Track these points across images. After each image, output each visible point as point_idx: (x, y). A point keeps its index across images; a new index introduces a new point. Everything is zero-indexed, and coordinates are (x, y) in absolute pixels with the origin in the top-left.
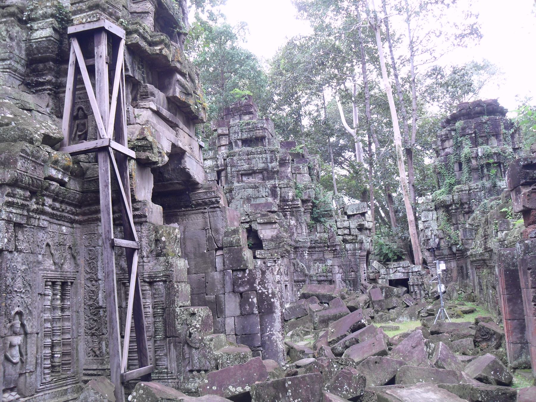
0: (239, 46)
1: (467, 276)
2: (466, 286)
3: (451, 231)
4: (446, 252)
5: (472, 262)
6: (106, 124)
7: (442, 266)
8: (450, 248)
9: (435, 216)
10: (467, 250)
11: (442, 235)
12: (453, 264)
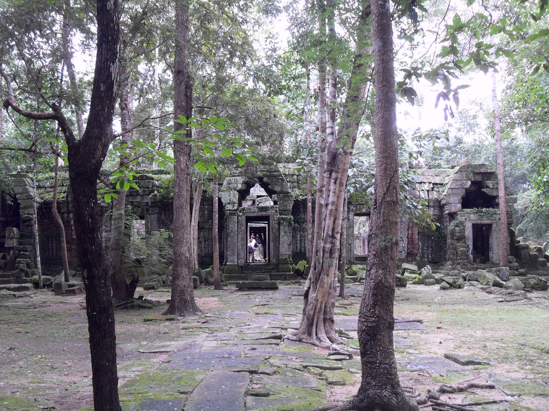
6: (255, 286)
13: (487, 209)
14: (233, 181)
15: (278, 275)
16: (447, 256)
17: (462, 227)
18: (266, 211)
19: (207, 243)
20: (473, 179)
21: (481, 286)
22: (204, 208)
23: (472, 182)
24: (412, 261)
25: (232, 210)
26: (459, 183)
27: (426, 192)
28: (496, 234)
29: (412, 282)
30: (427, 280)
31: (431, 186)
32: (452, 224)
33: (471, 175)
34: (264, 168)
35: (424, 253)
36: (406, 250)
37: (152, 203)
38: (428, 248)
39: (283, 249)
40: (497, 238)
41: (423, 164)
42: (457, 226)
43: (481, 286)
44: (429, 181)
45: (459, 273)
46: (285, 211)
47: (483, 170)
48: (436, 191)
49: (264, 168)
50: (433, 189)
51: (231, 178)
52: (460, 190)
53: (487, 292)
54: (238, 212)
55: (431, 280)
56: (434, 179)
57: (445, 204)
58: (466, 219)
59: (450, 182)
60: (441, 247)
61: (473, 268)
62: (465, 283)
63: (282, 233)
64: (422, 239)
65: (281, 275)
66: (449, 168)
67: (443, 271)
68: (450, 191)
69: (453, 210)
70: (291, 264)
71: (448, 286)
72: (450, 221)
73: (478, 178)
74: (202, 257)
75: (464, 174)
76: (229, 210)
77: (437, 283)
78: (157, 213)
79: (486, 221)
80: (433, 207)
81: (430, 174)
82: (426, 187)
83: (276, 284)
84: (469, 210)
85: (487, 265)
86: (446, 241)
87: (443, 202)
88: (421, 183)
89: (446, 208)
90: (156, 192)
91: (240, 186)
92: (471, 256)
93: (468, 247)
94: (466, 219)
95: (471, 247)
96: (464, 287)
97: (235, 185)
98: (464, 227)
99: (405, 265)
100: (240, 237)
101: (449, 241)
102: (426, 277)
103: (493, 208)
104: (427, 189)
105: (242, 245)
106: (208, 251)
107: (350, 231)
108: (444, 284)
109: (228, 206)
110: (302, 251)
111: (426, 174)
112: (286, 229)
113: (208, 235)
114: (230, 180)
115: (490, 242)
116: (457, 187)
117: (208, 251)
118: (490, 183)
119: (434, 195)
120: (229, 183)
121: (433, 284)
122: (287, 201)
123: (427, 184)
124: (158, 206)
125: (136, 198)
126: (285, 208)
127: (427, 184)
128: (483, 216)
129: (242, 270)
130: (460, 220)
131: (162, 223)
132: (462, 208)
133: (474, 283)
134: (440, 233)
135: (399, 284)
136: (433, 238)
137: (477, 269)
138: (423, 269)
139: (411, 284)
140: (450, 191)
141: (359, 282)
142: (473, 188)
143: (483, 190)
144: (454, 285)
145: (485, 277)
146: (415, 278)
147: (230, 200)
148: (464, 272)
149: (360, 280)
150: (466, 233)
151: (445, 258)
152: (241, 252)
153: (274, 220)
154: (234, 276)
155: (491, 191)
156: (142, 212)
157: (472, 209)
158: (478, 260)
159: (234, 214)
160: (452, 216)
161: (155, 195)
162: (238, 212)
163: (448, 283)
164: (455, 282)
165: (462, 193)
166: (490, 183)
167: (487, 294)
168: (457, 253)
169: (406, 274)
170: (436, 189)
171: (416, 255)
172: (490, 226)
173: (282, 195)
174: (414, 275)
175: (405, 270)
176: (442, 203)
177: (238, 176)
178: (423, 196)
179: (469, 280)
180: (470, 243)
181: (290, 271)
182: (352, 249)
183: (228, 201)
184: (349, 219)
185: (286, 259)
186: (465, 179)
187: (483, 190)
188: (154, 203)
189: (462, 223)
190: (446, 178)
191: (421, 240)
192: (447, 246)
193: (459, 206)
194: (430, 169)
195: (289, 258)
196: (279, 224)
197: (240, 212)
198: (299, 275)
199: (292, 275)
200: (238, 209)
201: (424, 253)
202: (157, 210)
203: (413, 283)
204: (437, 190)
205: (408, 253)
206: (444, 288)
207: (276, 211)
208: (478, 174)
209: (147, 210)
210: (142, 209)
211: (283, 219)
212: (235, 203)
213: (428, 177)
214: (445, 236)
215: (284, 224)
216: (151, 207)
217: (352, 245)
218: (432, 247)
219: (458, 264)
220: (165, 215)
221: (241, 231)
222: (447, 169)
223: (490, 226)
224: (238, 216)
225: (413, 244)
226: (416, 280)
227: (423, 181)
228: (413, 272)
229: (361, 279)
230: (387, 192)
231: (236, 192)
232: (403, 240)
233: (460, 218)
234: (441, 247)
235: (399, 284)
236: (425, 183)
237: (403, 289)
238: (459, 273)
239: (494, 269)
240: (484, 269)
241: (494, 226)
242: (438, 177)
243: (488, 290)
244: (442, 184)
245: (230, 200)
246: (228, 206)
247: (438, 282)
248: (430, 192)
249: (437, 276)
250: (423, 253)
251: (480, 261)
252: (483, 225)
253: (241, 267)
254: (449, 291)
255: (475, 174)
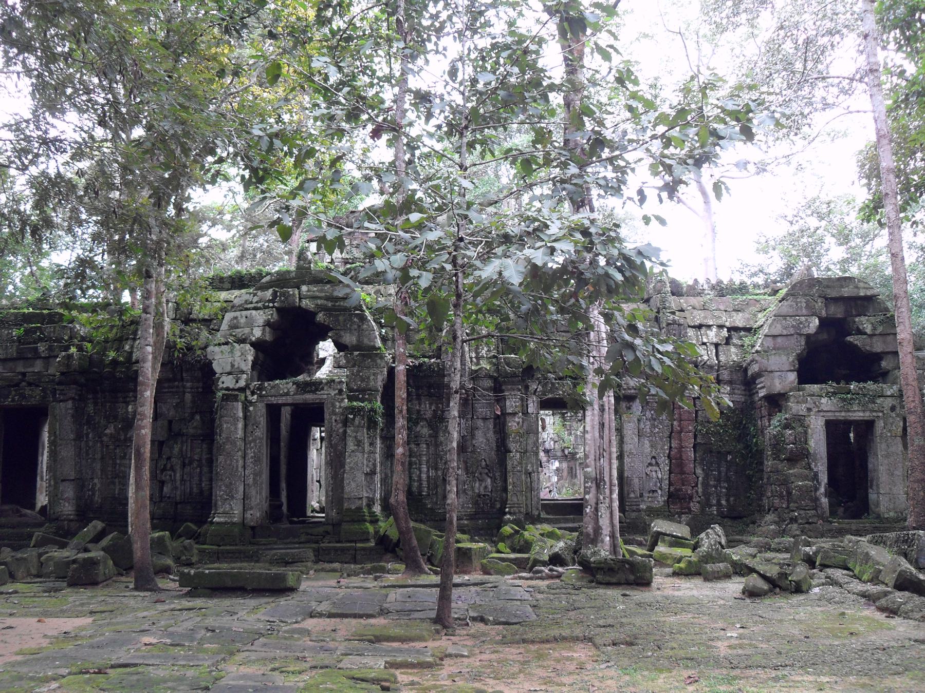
0: (731, 149)
1: (576, 476)
2: (574, 484)
3: (565, 435)
4: (559, 454)
5: (580, 464)
6: (229, 583)
7: (557, 464)
8: (563, 451)
9: (552, 421)
10: (576, 453)
11: (557, 439)
12: (565, 465)
13: (862, 385)
14: (243, 321)
15: (336, 550)
16: (765, 501)
17: (800, 429)
18: (314, 392)
19: (187, 469)
20: (824, 313)
21: (861, 587)
22: (184, 387)
23: (820, 319)
24: (680, 514)
25: (233, 390)
26: (791, 322)
27: (713, 348)
28: (884, 446)
29: (669, 570)
30: (709, 567)
31: (725, 333)
32: (775, 422)
33: (820, 304)
34: (321, 291)
35: (710, 494)
36: (666, 487)
37: (62, 374)
38: (718, 480)
39: (353, 485)
40: (887, 456)
41: (706, 287)
42: (787, 426)
43: (861, 587)
44: (720, 322)
45: (796, 544)
46: (363, 391)
47: (847, 292)
48: (735, 345)
49: (321, 291)
50: (728, 341)
51: (238, 314)
52: (793, 340)
53: (882, 609)
54: (248, 393)
55: (721, 566)
56: (731, 317)
57: (758, 375)
58: (809, 410)
59: (770, 321)
60: (749, 478)
61: (830, 531)
62: (812, 577)
63: (351, 446)
64: (703, 460)
65: (343, 550)
66: (765, 294)
67: (755, 539)
68: (770, 343)
69: (778, 386)
70: (372, 522)
71: (765, 586)
72: (770, 415)
73: (837, 311)
74: (177, 503)
75: (802, 302)
76: (227, 389)
77: (736, 573)
78: (73, 399)
79: (858, 414)
80: (730, 383)
81: (722, 308)
82: (712, 335)
83: (282, 578)
84: (815, 388)
85: (865, 522)
86: (762, 463)
87: (755, 368)
88: (700, 327)
89: (761, 382)
90: (73, 350)
91: (257, 333)
92: (824, 501)
93: (816, 477)
94: (809, 410)
95: (824, 478)
96: (810, 587)
97: (247, 330)
98: (806, 428)
99: (660, 525)
100: (250, 454)
101: (769, 463)
102: (708, 558)
103: (875, 380)
104: (715, 340)
105: (255, 475)
106: (191, 488)
107: (530, 442)
108: (754, 581)
109: (224, 378)
110: (414, 489)
111: (714, 306)
112: (364, 434)
113: (191, 450)
114: (236, 318)
115: (870, 466)
116: (785, 332)
117: (191, 488)
118: (866, 323)
119: (732, 355)
120: (233, 326)
121: (727, 576)
122: (368, 368)
123: (714, 329)
124: (75, 382)
125: (32, 366)
126: (363, 385)
127: (714, 329)
128: (849, 402)
129: (254, 536)
130: (794, 411)
131: (88, 422)
132: (800, 383)
133: (838, 574)
134: (747, 447)
135: (632, 577)
136: (729, 457)
137: (841, 533)
138: (703, 535)
139: (668, 576)
140: (770, 343)
141: (531, 570)
142: (824, 336)
143: (849, 339)
144: (784, 583)
145: (867, 557)
146: (679, 561)
147: (233, 366)
148: (809, 544)
149: (534, 565)
150: (812, 443)
151: (760, 506)
152: (253, 491)
153: (334, 413)
154: (228, 552)
155: (868, 340)
156: (44, 397)
157: (824, 386)
158: (841, 510)
159: (235, 398)
160: (776, 401)
161: (70, 357)
162: (248, 393)
163: (763, 577)
164: (784, 576)
165: (799, 346)
166: (866, 323)
167: (880, 616)
168: (789, 493)
169: (661, 548)
170: (735, 341)
171: (691, 498)
172: (869, 425)
173: (356, 353)
174: (678, 552)
175: (658, 537)
176: (750, 373)
177: (256, 309)
178: (706, 358)
179: (824, 566)
180: (821, 468)
181: (368, 540)
182: (535, 485)
183: (228, 369)
184: (526, 413)
185: (359, 509)
186: (804, 312)
187: (849, 339)
188: (68, 376)
189: (800, 420)
190: (760, 315)
191: (701, 464)
192: (765, 476)
193: (792, 377)
194: (723, 296)
195: (369, 506)
196: (346, 422)
197: (253, 393)
198: (387, 550)
199: (371, 549)
200: (247, 386)
201: (710, 494)
202: (72, 392)
203: (676, 574)
204: (739, 342)
205: (671, 495)
206: (751, 593)
207: (341, 391)
208: (836, 300)
209: (54, 392)
210: (44, 390)
211: (352, 410)
212: (243, 372)
213: (716, 313)
214: (761, 452)
215: (357, 422)
216: (60, 383)
217: (534, 475)
218: (728, 480)
219: (793, 520)
220: (96, 404)
221: (254, 441)
222: (762, 297)
223: (869, 425)
224: (247, 404)
225: (682, 473)
226: (682, 565)
227: (705, 322)
228: (677, 542)
229: (536, 562)
230: (848, 569)
231: (248, 346)
232: (657, 464)
233: (795, 407)
234: (749, 478)
235: (632, 577)
236: (709, 327)
237: (638, 595)
238: (796, 544)
239: (892, 535)
240: (858, 533)
241: (880, 424)
242: (740, 314)
243: (883, 602)
244: (748, 330)
245: (233, 366)
246: (224, 378)
247: (741, 570)
248: (720, 348)
249: (737, 554)
250: (706, 494)
251: (844, 513)
252: (848, 424)
253: (253, 528)
254: (767, 601)
255: (829, 300)
